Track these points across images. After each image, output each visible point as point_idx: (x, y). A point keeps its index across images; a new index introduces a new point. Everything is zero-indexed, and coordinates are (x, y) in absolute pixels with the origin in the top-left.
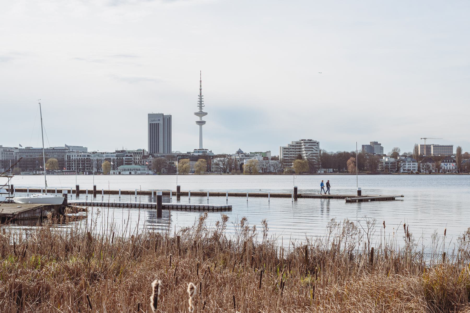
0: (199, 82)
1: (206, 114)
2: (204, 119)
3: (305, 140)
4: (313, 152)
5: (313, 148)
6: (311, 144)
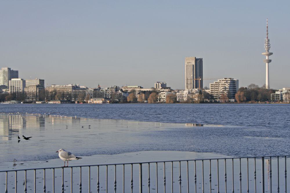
5: (225, 84)
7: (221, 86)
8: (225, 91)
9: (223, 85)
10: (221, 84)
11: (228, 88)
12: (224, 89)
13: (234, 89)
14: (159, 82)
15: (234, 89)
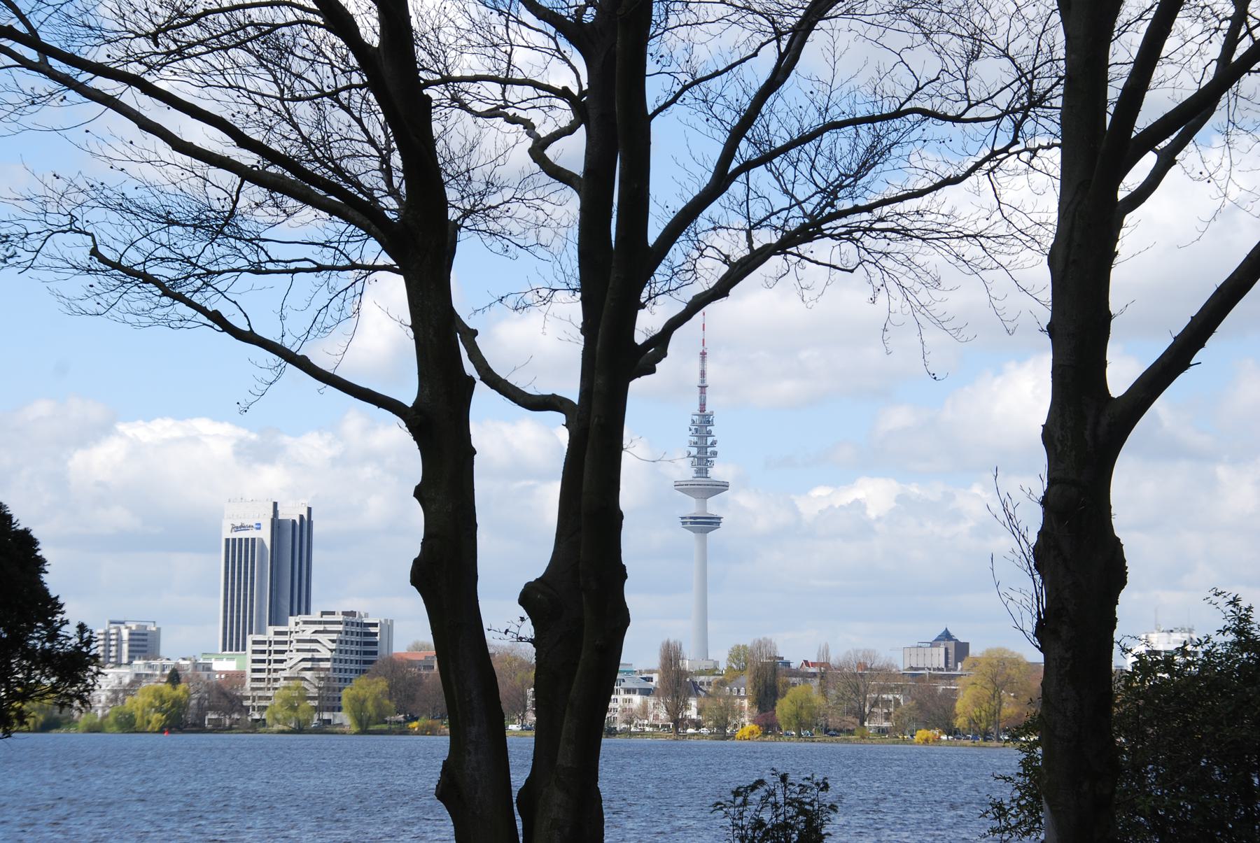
0: (698, 358)
1: (722, 487)
2: (713, 507)
3: (333, 613)
4: (317, 656)
5: (317, 641)
6: (321, 627)
7: (298, 650)
8: (308, 675)
9: (307, 646)
10: (299, 641)
11: (328, 660)
12: (309, 665)
13: (366, 653)
14: (123, 623)
15: (366, 653)
